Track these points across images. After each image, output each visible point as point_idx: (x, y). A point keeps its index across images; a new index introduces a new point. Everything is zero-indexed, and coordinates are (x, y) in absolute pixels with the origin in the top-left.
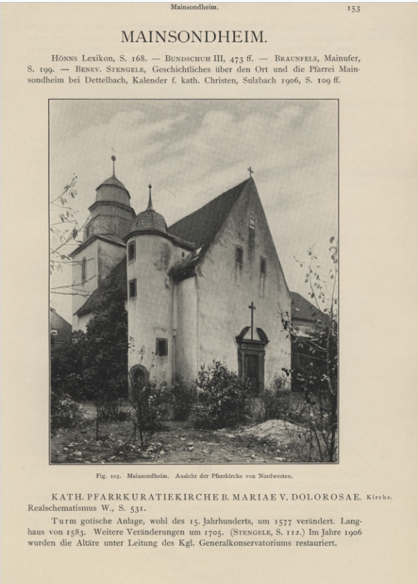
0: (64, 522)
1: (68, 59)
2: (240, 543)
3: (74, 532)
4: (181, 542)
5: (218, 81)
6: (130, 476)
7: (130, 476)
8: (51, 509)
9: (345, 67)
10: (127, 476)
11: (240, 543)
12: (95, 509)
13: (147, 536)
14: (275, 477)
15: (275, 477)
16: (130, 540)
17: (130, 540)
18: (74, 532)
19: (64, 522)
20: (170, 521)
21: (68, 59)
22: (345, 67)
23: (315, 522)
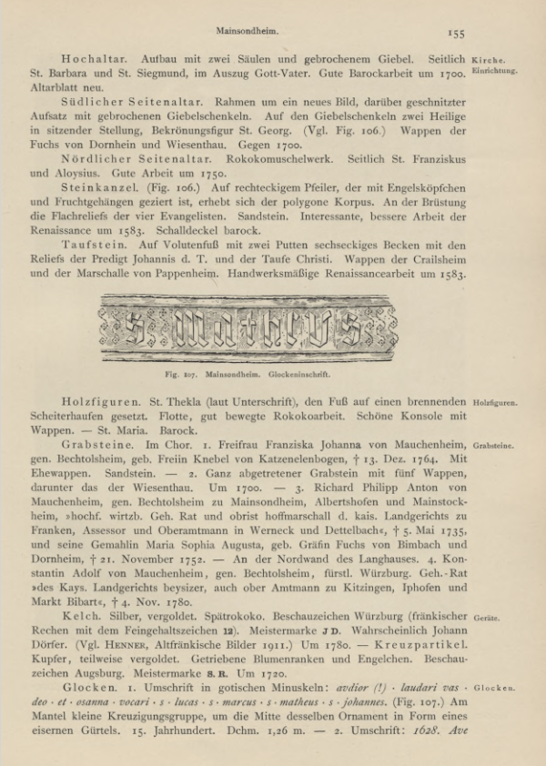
0: (117, 403)
1: (127, 645)
2: (418, 417)
3: (129, 231)
4: (34, 659)
5: (213, 660)
6: (209, 374)
7: (209, 374)
8: (445, 660)
9: (142, 570)
10: (205, 374)
11: (418, 417)
12: (156, 589)
13: (366, 721)
14: (310, 160)
15: (310, 160)
16: (95, 584)
17: (95, 584)
18: (129, 231)
19: (117, 403)
20: (444, 246)
21: (127, 645)
22: (142, 570)
23: (437, 103)
